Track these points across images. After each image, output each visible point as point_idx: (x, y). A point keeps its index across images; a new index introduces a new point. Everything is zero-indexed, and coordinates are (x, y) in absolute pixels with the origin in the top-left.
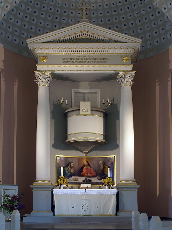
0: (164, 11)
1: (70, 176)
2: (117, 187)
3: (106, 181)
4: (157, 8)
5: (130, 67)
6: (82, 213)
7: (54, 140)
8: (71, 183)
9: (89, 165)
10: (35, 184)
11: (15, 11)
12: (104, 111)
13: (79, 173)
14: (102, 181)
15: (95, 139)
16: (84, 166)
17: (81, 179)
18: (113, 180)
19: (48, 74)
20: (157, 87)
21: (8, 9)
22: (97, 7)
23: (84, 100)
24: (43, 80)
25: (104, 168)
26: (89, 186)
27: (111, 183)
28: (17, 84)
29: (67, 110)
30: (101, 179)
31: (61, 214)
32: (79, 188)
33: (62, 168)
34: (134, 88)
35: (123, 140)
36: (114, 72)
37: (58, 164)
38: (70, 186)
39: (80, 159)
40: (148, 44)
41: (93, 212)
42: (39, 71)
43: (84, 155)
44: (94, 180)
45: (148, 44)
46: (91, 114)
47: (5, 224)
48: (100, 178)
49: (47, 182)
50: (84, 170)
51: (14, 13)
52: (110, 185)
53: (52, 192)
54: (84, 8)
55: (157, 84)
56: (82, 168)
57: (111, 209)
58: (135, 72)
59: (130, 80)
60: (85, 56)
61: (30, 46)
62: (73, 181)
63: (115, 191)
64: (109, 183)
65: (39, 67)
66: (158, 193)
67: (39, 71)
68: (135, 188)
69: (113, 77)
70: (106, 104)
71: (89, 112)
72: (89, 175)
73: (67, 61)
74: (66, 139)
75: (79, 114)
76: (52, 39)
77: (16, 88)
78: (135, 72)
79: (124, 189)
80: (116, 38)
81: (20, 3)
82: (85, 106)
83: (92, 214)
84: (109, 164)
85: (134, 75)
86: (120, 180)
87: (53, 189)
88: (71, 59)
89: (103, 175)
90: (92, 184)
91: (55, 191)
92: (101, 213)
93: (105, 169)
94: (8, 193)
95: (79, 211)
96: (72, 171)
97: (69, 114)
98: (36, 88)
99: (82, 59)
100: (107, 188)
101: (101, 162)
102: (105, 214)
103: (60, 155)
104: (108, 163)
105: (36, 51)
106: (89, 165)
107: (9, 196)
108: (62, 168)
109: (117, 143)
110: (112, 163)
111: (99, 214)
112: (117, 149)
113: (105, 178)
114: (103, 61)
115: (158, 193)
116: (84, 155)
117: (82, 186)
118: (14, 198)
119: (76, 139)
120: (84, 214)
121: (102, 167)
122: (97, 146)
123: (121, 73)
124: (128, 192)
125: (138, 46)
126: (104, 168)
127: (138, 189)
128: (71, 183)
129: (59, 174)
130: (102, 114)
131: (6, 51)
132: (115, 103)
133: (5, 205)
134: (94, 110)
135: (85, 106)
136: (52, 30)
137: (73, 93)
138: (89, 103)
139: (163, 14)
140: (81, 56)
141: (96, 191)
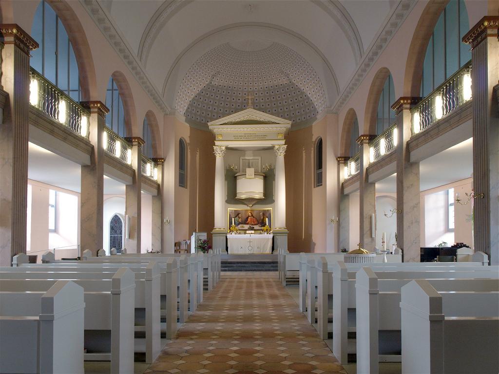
0: (309, 96)
1: (239, 224)
2: (273, 233)
3: (265, 228)
4: (304, 93)
5: (283, 142)
6: (248, 252)
7: (226, 197)
8: (240, 230)
9: (252, 215)
10: (214, 231)
11: (198, 97)
12: (264, 175)
13: (245, 222)
14: (263, 228)
15: (257, 196)
16: (249, 216)
17: (246, 227)
18: (270, 227)
19: (224, 148)
20: (304, 154)
21: (193, 97)
22: (259, 88)
23: (249, 167)
24: (220, 152)
25: (264, 218)
26: (253, 232)
27: (269, 230)
28: (198, 153)
29: (236, 173)
30: (261, 227)
31: (232, 253)
32: (245, 233)
33: (233, 219)
34: (286, 157)
35: (277, 196)
36: (271, 145)
37: (230, 215)
38: (239, 232)
39: (247, 211)
40: (298, 119)
41: (256, 251)
42: (217, 146)
43: (249, 208)
44: (256, 227)
45: (298, 119)
46: (255, 177)
47: (135, 287)
48: (260, 225)
49: (222, 229)
50: (249, 220)
51: (197, 98)
52: (268, 231)
53: (226, 237)
54: (250, 97)
55: (304, 151)
56: (247, 218)
57: (268, 250)
58: (286, 146)
59: (283, 152)
60: (250, 134)
61: (210, 127)
62: (240, 228)
63: (271, 236)
64: (267, 230)
65: (217, 143)
66: (303, 237)
67: (217, 146)
68: (286, 233)
69: (271, 148)
70: (265, 169)
71: (253, 176)
72: (252, 223)
73: (237, 138)
74: (236, 196)
75: (246, 177)
76: (226, 121)
77: (198, 156)
78: (286, 146)
79: (278, 235)
80: (273, 121)
81: (201, 91)
82: (250, 172)
83: (255, 253)
84: (267, 215)
85: (285, 148)
86: (345, 253)
87: (226, 234)
88: (240, 136)
89: (263, 224)
90: (255, 230)
91: (228, 236)
92: (261, 252)
93: (265, 219)
94: (200, 238)
95: (245, 251)
96: (240, 220)
97: (238, 178)
98: (214, 158)
99: (248, 136)
100: (266, 233)
101: (261, 213)
102: (264, 253)
103: (233, 208)
104: (266, 214)
105: (215, 131)
106: (252, 215)
107: (201, 240)
108: (233, 219)
109: (274, 199)
110: (270, 214)
111: (259, 253)
112: (273, 204)
113: (264, 226)
114: (263, 137)
115: (303, 237)
116: (249, 208)
117: (247, 232)
118: (205, 241)
119: (243, 197)
120: (250, 253)
121: (262, 217)
122: (259, 201)
123: (277, 147)
124: (42, 35)
125: (289, 126)
126: (264, 218)
127: (288, 234)
128: (240, 230)
129: (231, 223)
130: (262, 177)
131: (191, 129)
132: (273, 167)
133: (200, 246)
134: (257, 174)
135: (250, 172)
136: (228, 114)
137: (241, 160)
138: (253, 169)
139: (308, 98)
140: (247, 134)
141: (257, 236)
